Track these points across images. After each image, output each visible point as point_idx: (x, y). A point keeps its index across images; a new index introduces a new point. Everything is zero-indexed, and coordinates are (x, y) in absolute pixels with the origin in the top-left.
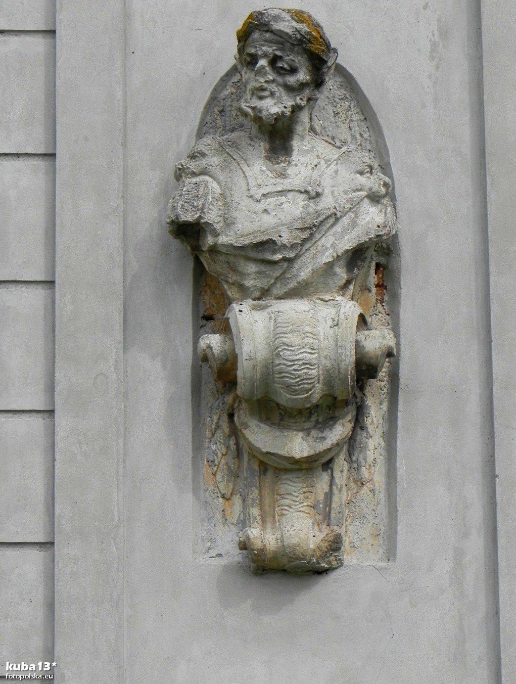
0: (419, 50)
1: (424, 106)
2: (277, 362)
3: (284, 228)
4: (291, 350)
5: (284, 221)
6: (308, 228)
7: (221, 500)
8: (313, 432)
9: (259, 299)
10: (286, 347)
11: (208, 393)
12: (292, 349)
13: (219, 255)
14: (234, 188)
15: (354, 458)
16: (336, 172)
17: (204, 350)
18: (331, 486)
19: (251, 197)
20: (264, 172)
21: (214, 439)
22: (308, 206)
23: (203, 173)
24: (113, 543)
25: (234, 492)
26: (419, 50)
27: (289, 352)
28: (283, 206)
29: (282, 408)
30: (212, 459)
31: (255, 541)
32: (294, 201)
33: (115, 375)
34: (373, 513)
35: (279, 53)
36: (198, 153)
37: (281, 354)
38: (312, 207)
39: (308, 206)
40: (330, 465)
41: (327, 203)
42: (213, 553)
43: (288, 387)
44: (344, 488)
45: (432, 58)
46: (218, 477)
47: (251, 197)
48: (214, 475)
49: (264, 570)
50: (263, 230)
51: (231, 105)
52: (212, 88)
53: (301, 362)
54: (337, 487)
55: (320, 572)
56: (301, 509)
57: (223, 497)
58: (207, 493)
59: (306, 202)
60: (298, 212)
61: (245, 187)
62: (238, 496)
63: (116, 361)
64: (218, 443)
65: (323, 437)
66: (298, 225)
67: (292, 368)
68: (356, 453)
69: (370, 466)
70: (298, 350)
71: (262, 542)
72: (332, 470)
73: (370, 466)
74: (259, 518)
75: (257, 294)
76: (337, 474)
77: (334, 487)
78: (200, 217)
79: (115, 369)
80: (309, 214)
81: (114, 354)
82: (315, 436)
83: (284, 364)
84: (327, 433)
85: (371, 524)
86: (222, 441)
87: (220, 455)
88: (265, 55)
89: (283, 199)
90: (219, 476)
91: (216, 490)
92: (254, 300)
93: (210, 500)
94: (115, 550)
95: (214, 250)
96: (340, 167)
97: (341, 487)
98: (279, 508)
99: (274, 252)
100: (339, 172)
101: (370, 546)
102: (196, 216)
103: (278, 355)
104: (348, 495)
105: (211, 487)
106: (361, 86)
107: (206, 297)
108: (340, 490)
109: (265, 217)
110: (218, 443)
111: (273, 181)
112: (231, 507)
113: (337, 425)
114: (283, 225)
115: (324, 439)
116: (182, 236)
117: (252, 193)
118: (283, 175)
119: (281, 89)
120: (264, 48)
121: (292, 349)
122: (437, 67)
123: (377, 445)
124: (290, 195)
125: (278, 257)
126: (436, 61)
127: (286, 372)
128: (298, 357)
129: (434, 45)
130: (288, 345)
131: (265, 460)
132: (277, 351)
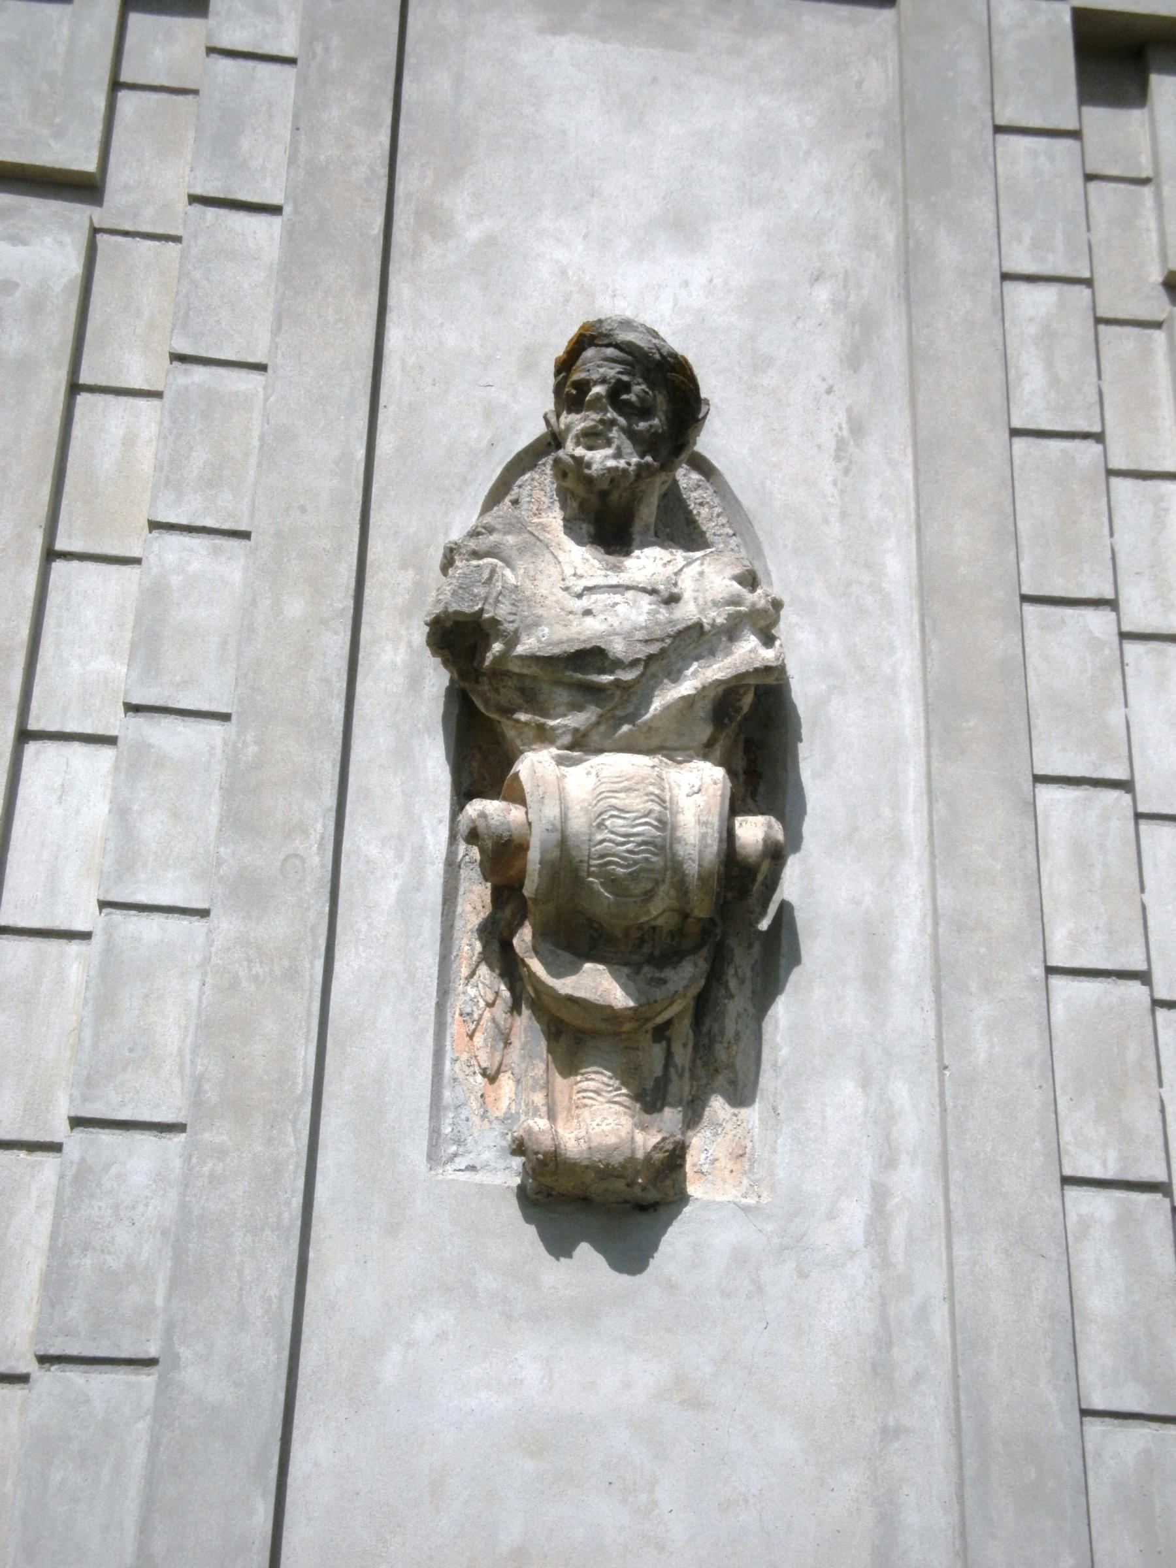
0: (819, 447)
1: (826, 521)
2: (599, 837)
3: (618, 639)
4: (624, 818)
5: (618, 629)
6: (657, 640)
7: (479, 1078)
8: (646, 969)
9: (568, 748)
10: (616, 813)
11: (469, 908)
12: (627, 815)
13: (506, 678)
14: (539, 577)
15: (705, 1030)
16: (701, 574)
17: (473, 821)
18: (666, 1067)
19: (566, 589)
20: (587, 560)
21: (472, 980)
22: (658, 612)
23: (488, 554)
24: (290, 1128)
25: (503, 1068)
26: (819, 447)
27: (621, 822)
28: (616, 608)
29: (596, 925)
30: (468, 1010)
31: (542, 1138)
32: (635, 601)
33: (317, 859)
34: (735, 1119)
35: (625, 378)
36: (485, 528)
37: (608, 823)
38: (663, 614)
39: (658, 612)
40: (668, 1033)
41: (687, 612)
42: (461, 1163)
43: (613, 881)
44: (687, 1074)
45: (838, 458)
46: (475, 1039)
47: (566, 589)
48: (471, 1036)
49: (549, 1195)
50: (583, 638)
51: (530, 495)
52: (503, 465)
53: (639, 839)
54: (676, 1071)
55: (644, 1208)
56: (617, 1099)
57: (484, 1074)
58: (457, 1065)
59: (653, 607)
60: (642, 619)
61: (556, 577)
62: (509, 1074)
63: (322, 838)
64: (480, 985)
65: (661, 979)
66: (639, 635)
67: (624, 848)
68: (708, 1022)
69: (729, 1043)
70: (636, 818)
71: (553, 1139)
72: (669, 1041)
73: (729, 1043)
74: (544, 1109)
75: (567, 739)
76: (677, 1048)
77: (672, 1070)
78: (482, 610)
79: (319, 849)
80: (658, 623)
81: (319, 827)
82: (649, 976)
83: (611, 841)
84: (668, 973)
85: (730, 1136)
86: (487, 982)
87: (482, 1004)
88: (603, 381)
89: (618, 598)
90: (479, 1039)
91: (473, 1062)
92: (558, 748)
93: (461, 1076)
94: (292, 1141)
95: (499, 673)
96: (707, 569)
97: (683, 1071)
98: (580, 1095)
99: (602, 671)
100: (706, 575)
101: (727, 1173)
102: (477, 608)
103: (601, 826)
104: (692, 1086)
105: (465, 1056)
106: (731, 484)
107: (475, 764)
108: (681, 1076)
109: (589, 620)
110: (480, 985)
111: (603, 572)
112: (495, 1091)
113: (684, 963)
114: (617, 634)
115: (663, 982)
116: (447, 651)
117: (568, 583)
118: (617, 568)
119: (623, 437)
120: (602, 370)
121: (627, 815)
122: (846, 472)
123: (741, 1011)
124: (630, 594)
125: (606, 678)
126: (844, 463)
127: (613, 855)
128: (635, 830)
129: (841, 445)
130: (618, 810)
131: (564, 1015)
132: (599, 820)
